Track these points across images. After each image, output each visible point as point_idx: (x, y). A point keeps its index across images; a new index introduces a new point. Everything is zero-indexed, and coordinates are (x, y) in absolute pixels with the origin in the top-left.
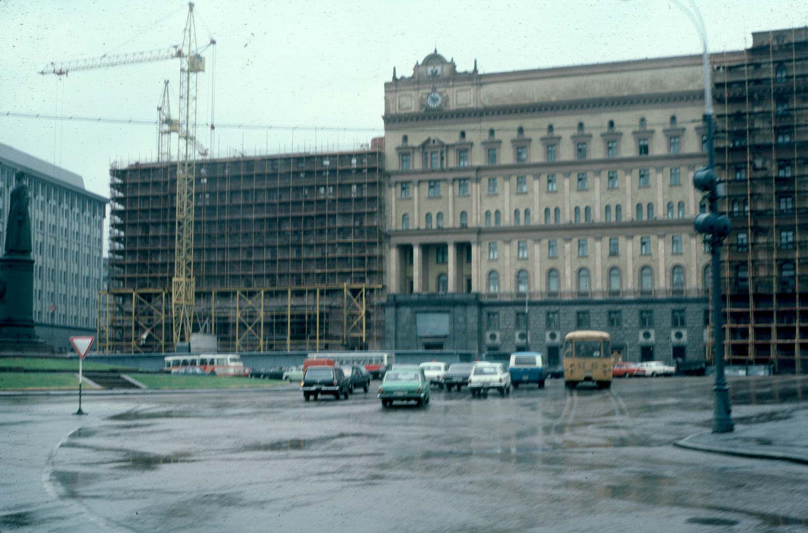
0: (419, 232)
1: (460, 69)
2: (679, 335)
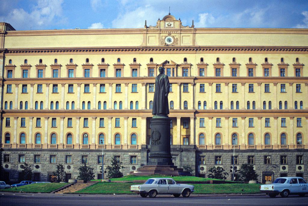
2: (300, 168)
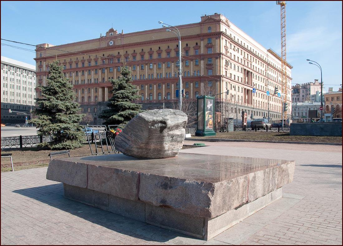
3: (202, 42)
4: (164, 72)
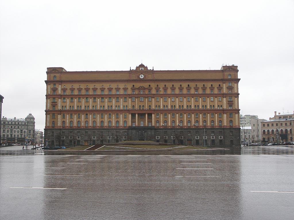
0: (137, 110)
1: (149, 69)
3: (224, 85)
4: (193, 104)
